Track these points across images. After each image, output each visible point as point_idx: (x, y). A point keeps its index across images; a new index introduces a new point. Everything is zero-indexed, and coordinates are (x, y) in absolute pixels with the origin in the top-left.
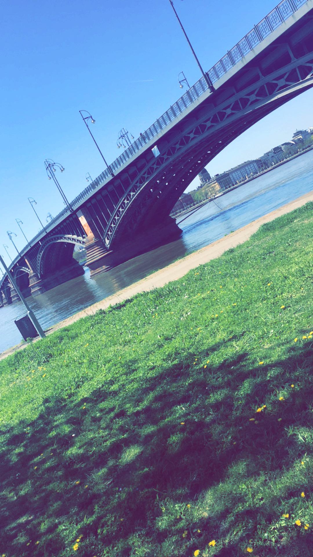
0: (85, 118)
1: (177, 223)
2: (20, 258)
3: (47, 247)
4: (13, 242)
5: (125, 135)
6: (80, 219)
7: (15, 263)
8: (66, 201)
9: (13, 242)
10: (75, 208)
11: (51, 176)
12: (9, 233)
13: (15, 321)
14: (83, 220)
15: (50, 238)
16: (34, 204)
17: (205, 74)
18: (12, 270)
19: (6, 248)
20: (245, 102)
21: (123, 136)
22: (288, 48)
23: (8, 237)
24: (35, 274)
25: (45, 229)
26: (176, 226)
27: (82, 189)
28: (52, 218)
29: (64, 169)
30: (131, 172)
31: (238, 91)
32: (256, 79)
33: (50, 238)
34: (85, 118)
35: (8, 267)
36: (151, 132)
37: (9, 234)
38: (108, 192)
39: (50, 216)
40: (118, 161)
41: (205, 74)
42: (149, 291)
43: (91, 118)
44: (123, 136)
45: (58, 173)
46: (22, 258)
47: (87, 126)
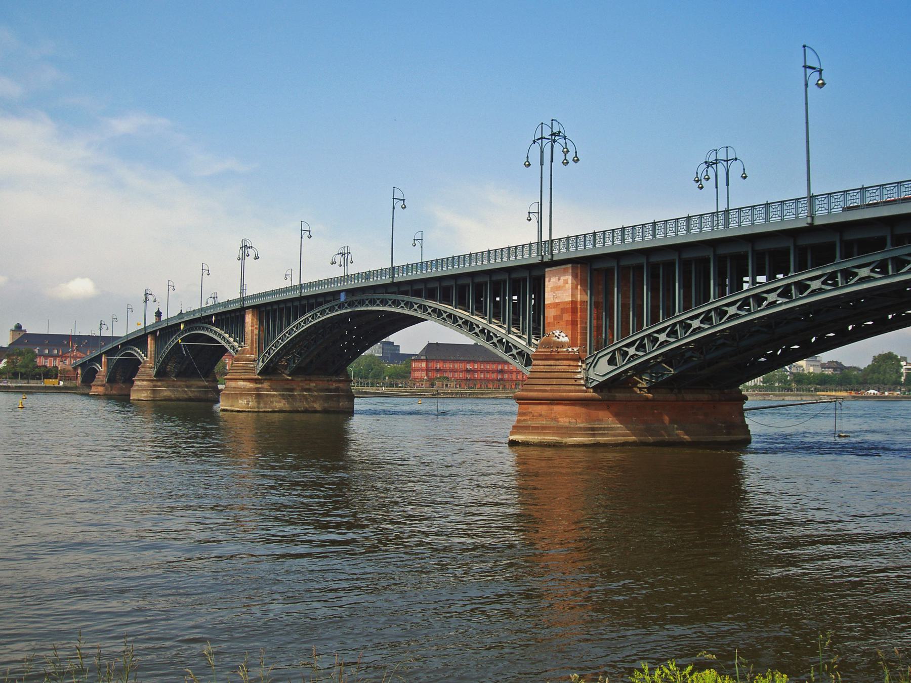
1: (745, 406)
2: (143, 333)
5: (346, 255)
7: (208, 313)
8: (242, 290)
10: (247, 304)
11: (241, 257)
13: (18, 327)
18: (182, 326)
19: (205, 273)
21: (343, 254)
22: (645, 261)
23: (238, 252)
26: (741, 412)
28: (215, 301)
29: (576, 160)
36: (386, 273)
37: (101, 324)
38: (293, 305)
39: (214, 298)
40: (311, 285)
42: (23, 328)
43: (818, 73)
44: (343, 254)
45: (249, 261)
47: (806, 85)
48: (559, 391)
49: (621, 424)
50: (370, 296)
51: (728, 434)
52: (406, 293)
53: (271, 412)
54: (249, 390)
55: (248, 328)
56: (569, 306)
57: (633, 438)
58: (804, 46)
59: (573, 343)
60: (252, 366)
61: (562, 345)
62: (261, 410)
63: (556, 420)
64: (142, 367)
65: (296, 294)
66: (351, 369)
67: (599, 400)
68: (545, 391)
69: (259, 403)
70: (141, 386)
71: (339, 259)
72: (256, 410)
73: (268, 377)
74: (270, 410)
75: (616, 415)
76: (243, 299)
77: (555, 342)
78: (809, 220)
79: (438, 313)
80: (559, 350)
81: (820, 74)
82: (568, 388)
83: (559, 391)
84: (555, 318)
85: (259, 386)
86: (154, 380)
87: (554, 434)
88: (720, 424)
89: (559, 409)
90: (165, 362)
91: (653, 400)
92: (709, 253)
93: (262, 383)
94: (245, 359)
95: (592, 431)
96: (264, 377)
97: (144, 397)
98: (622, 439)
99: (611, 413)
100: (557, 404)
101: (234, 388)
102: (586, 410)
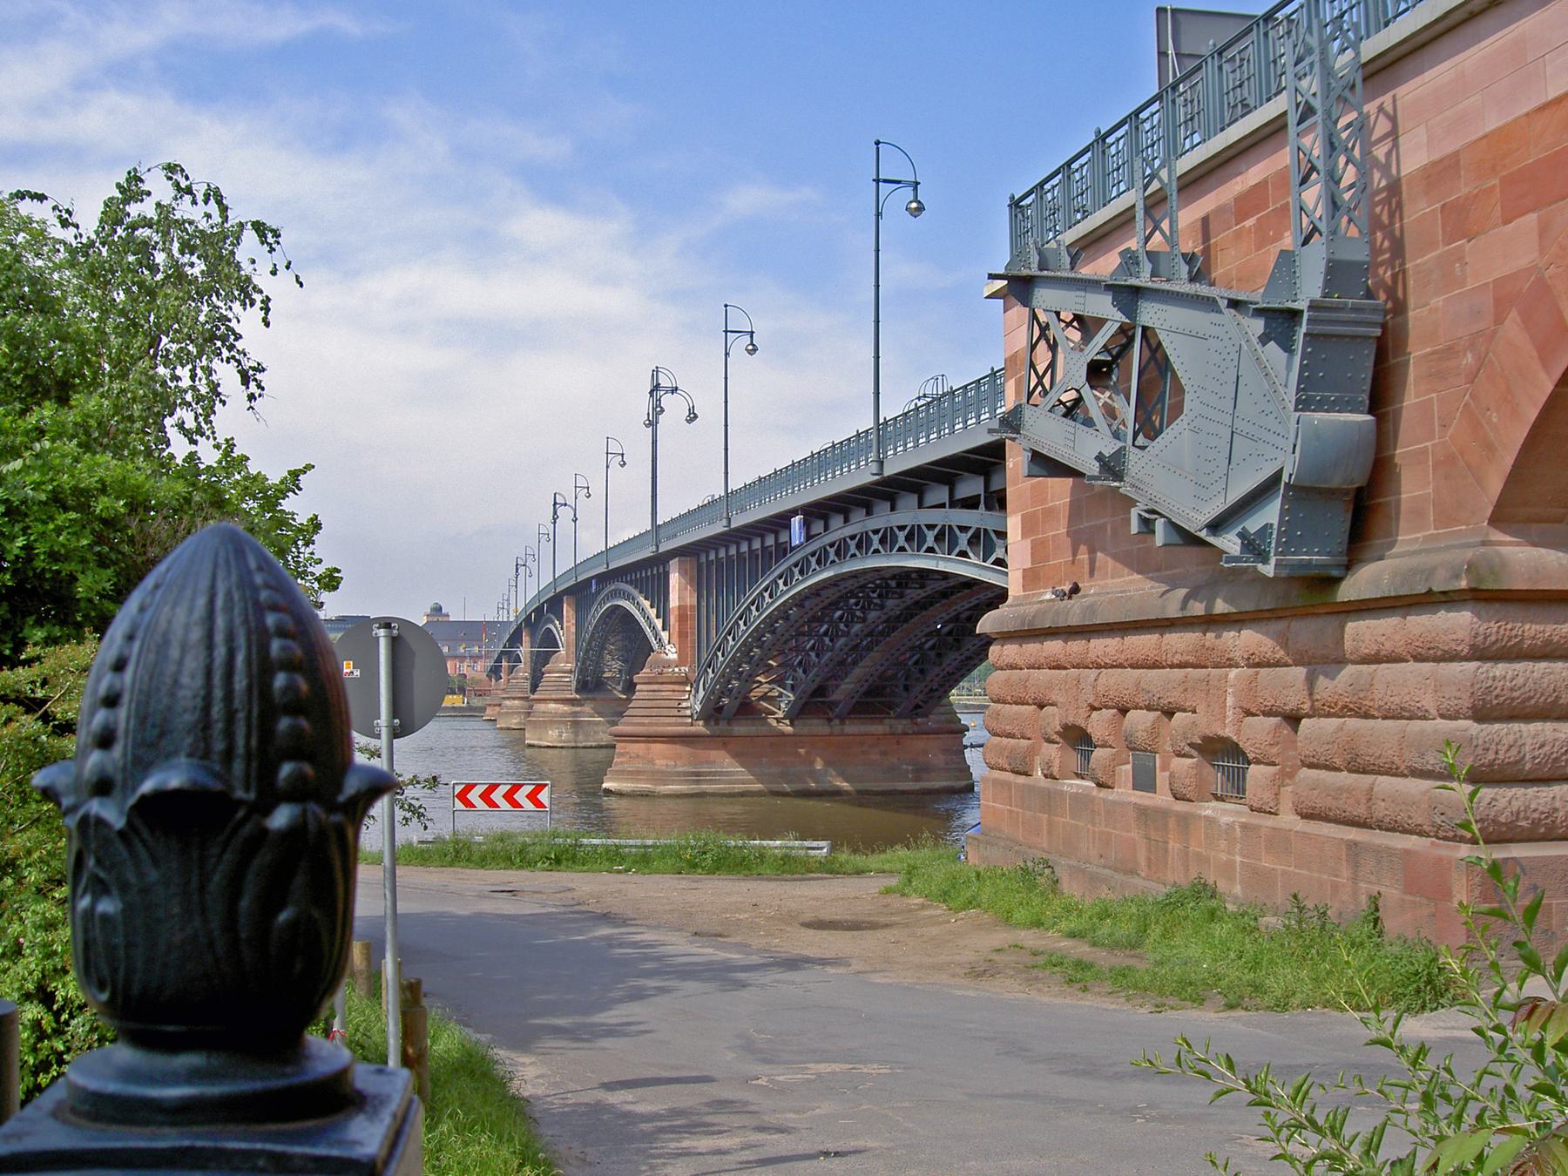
0: (885, 181)
1: (965, 741)
3: (816, 590)
4: (654, 443)
6: (671, 576)
9: (654, 443)
12: (664, 382)
15: (940, 517)
17: (881, 421)
31: (954, 504)
33: (940, 517)
34: (885, 181)
35: (659, 522)
37: (656, 388)
40: (763, 486)
41: (729, 491)
43: (748, 337)
46: (659, 562)
47: (878, 215)
48: (657, 725)
49: (742, 767)
51: (917, 779)
53: (595, 747)
54: (563, 715)
57: (759, 786)
58: (877, 143)
59: (681, 661)
60: (567, 680)
61: (668, 664)
62: (579, 745)
63: (652, 762)
64: (514, 679)
67: (708, 736)
68: (643, 724)
69: (576, 734)
70: (511, 707)
72: (573, 744)
73: (590, 696)
74: (594, 744)
75: (739, 756)
77: (663, 660)
80: (665, 670)
81: (752, 337)
82: (667, 720)
83: (657, 725)
85: (578, 709)
86: (576, 700)
87: (647, 781)
88: (905, 767)
89: (657, 748)
90: (751, 658)
91: (794, 735)
93: (582, 705)
94: (557, 669)
95: (697, 776)
96: (585, 696)
97: (516, 724)
98: (739, 787)
99: (729, 752)
100: (655, 742)
101: (544, 712)
102: (687, 749)
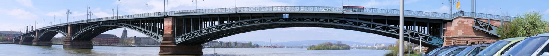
6: (69, 28)
8: (68, 20)
10: (69, 24)
14: (69, 28)
16: (89, 8)
20: (118, 25)
23: (35, 22)
24: (70, 36)
25: (43, 28)
27: (58, 24)
30: (92, 23)
32: (356, 19)
33: (112, 23)
50: (108, 23)
52: (120, 22)
55: (36, 34)
56: (171, 26)
65: (42, 29)
66: (52, 39)
71: (50, 23)
76: (36, 30)
78: (342, 12)
79: (61, 32)
84: (167, 29)
92: (151, 19)
